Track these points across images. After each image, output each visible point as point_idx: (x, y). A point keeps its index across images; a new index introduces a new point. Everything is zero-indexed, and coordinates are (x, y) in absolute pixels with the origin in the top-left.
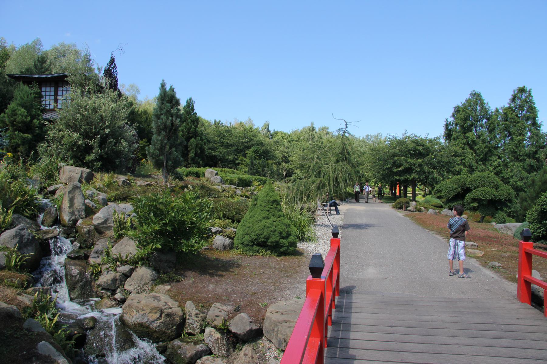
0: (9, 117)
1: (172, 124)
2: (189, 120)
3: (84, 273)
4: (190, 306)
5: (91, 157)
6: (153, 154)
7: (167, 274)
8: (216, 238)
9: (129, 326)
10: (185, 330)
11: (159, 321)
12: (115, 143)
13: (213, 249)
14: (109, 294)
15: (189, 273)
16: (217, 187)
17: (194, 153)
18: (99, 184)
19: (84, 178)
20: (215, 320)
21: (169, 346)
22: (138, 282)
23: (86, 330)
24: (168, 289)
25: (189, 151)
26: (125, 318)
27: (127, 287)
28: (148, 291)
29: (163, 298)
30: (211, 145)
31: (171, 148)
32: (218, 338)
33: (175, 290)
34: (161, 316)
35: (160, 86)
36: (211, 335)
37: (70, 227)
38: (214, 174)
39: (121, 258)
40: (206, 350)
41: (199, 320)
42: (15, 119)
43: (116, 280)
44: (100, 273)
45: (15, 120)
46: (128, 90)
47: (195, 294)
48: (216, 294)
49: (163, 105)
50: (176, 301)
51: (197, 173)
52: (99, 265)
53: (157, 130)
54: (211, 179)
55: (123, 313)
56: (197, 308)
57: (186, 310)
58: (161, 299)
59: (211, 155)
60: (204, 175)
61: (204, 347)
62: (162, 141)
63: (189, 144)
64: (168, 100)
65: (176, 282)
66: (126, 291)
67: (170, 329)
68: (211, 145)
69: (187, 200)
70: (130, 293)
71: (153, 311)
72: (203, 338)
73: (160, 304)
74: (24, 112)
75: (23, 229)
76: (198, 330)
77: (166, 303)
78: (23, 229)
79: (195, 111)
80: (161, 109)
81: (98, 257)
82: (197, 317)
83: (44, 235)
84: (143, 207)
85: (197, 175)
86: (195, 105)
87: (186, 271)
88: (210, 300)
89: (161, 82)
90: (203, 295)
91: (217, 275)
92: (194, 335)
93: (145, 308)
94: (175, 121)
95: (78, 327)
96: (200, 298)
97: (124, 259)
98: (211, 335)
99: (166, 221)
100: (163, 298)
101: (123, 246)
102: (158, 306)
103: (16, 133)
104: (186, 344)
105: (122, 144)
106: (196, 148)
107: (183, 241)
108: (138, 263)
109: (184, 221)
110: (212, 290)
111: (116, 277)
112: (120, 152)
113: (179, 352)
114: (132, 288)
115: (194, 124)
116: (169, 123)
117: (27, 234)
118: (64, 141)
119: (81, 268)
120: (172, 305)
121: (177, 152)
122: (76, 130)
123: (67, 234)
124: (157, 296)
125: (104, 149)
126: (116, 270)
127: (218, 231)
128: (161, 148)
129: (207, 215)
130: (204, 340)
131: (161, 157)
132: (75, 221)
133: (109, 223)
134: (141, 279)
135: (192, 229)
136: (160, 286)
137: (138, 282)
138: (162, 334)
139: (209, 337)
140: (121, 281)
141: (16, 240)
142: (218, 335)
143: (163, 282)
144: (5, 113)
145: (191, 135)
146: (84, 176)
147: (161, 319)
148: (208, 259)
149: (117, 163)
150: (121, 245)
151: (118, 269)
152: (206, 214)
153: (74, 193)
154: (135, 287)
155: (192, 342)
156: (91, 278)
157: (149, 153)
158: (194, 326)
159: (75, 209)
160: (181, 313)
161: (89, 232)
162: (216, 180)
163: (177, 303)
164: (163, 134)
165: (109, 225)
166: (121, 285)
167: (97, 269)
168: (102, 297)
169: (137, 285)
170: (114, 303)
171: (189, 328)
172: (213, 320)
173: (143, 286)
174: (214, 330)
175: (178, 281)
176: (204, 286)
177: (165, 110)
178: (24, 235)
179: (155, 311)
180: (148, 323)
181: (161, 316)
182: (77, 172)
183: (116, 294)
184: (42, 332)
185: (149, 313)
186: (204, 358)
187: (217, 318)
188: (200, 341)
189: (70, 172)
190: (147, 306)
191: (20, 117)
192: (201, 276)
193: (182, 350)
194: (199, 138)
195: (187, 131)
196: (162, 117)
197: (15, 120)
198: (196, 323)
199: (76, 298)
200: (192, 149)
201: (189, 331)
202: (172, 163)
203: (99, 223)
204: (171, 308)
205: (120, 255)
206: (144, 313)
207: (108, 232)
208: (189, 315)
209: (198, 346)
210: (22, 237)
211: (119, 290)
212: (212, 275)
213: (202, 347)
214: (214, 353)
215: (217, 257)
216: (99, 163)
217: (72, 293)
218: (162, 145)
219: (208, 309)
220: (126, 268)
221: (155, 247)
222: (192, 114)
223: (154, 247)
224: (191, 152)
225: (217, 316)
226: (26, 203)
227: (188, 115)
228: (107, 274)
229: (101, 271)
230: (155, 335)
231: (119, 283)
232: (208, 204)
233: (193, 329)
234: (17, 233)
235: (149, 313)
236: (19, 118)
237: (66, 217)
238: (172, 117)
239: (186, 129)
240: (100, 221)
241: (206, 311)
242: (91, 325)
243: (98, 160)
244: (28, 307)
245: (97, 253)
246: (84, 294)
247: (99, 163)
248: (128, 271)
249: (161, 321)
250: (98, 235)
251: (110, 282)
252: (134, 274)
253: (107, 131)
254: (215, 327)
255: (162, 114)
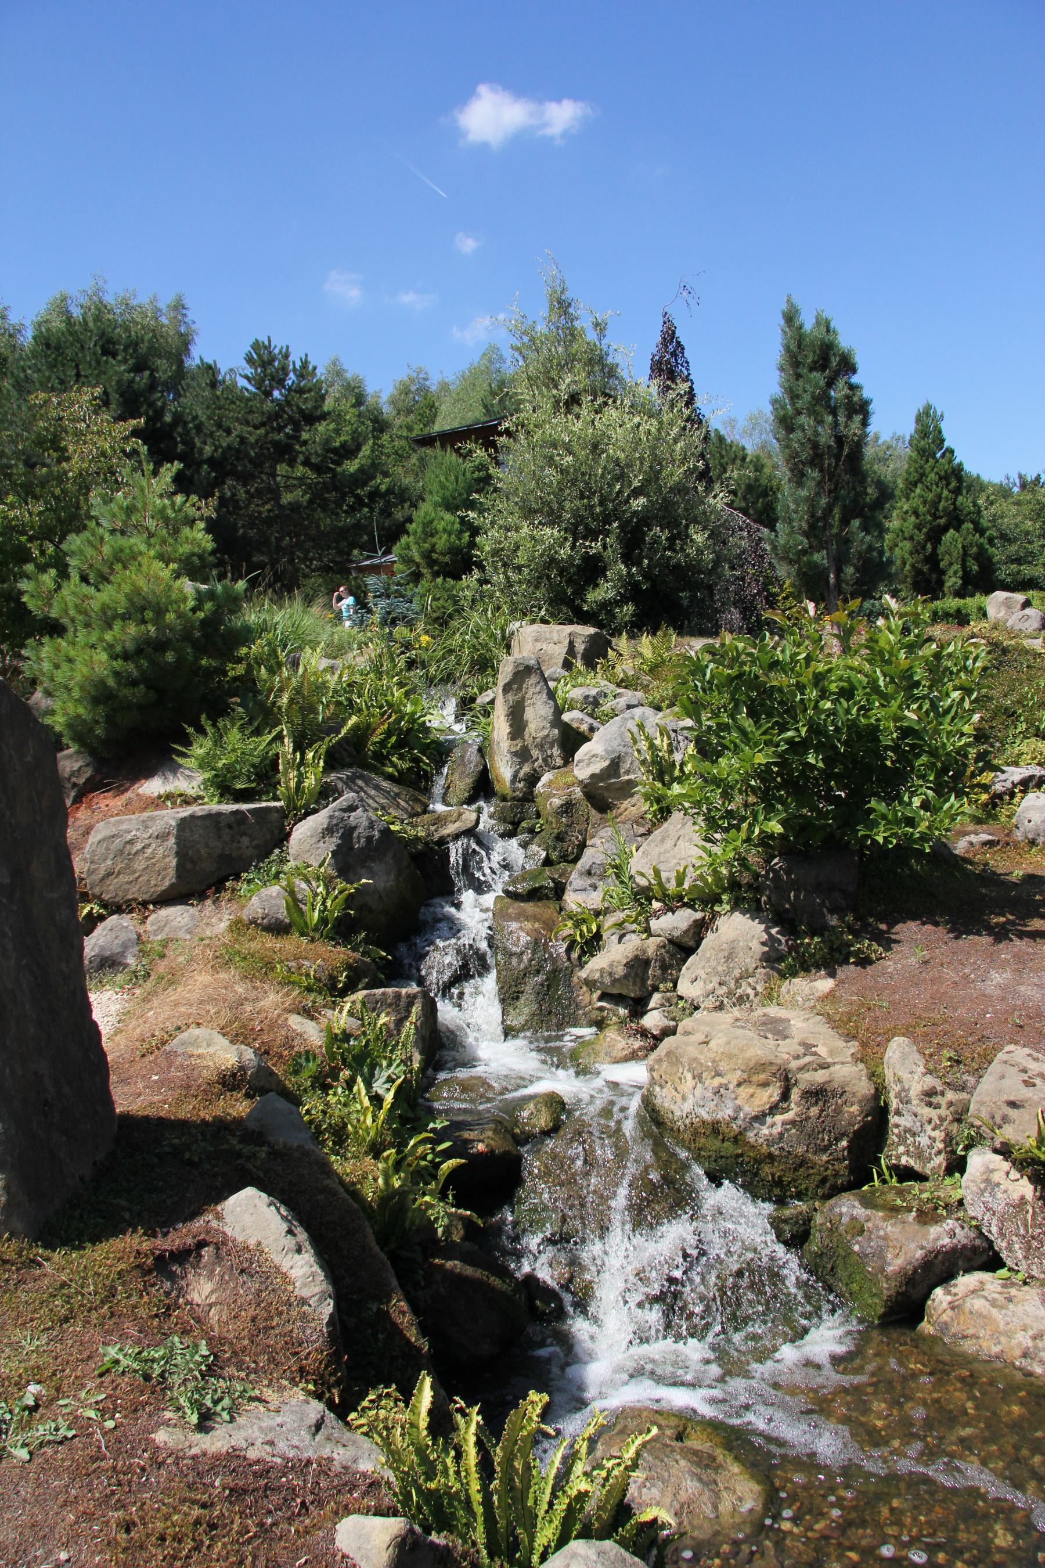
0: (417, 543)
1: (840, 440)
2: (932, 476)
3: (546, 944)
4: (904, 1057)
5: (603, 592)
6: (787, 550)
7: (821, 935)
8: (1024, 803)
9: (675, 1132)
10: (889, 1157)
11: (779, 1118)
12: (671, 540)
13: (1016, 844)
14: (623, 1011)
15: (908, 930)
16: (1030, 641)
17: (960, 574)
18: (625, 667)
19: (579, 656)
20: (1005, 1119)
21: (818, 1219)
22: (720, 969)
23: (524, 1139)
24: (827, 990)
25: (943, 572)
26: (658, 1101)
27: (684, 987)
28: (756, 1000)
29: (800, 1025)
30: (1013, 549)
31: (845, 522)
32: (1022, 1198)
33: (849, 996)
34: (785, 1096)
35: (782, 322)
36: (990, 1185)
37: (519, 800)
38: (1019, 606)
39: (660, 884)
40: (974, 1249)
41: (942, 1119)
42: (434, 545)
43: (647, 963)
44: (593, 944)
45: (433, 549)
46: (745, 432)
47: (926, 1009)
48: (1014, 1008)
49: (801, 383)
50: (850, 1037)
51: (959, 611)
52: (597, 913)
53: (792, 470)
54: (1009, 624)
55: (653, 1082)
56: (931, 1066)
57: (889, 1074)
58: (794, 1031)
59: (1020, 578)
60: (985, 615)
61: (964, 1236)
62: (811, 501)
63: (941, 549)
64: (814, 362)
65: (855, 964)
66: (681, 1004)
67: (825, 1149)
68: (1013, 549)
69: (881, 653)
70: (697, 1008)
71: (755, 1078)
72: (957, 1195)
73: (784, 1051)
74: (453, 524)
75: (352, 808)
76: (940, 1161)
77: (808, 1047)
78: (352, 808)
79: (946, 444)
80: (794, 396)
81: (595, 887)
82: (929, 1104)
83: (432, 828)
84: (711, 689)
85: (961, 618)
86: (943, 426)
87: (897, 922)
88: (986, 1033)
89: (784, 307)
90: (961, 1012)
91: (1021, 935)
92: (922, 1178)
93: (723, 1067)
94: (846, 426)
95: (495, 1131)
96: (946, 1027)
97: (672, 887)
98: (990, 1185)
99: (797, 730)
100: (800, 1025)
101: (669, 843)
102: (771, 1058)
103: (439, 580)
104: (884, 1219)
105: (692, 540)
106: (964, 561)
107: (873, 803)
108: (720, 902)
109: (874, 731)
110: (998, 992)
111: (644, 952)
112: (689, 566)
113: (856, 1248)
114: (699, 993)
115: (948, 484)
116: (825, 436)
117: (365, 823)
118: (522, 558)
119: (537, 925)
120: (831, 1053)
121: (868, 532)
122: (554, 519)
123: (512, 823)
124: (780, 1020)
125: (639, 564)
126: (647, 930)
127: (1031, 777)
128: (812, 526)
129: (962, 700)
130: (961, 1203)
131: (816, 557)
132: (533, 779)
133: (628, 772)
134: (729, 958)
135: (905, 758)
136: (796, 981)
137: (720, 969)
138: (796, 1170)
139: (983, 1191)
140: (664, 967)
141: (332, 843)
142: (1025, 1188)
143: (804, 966)
144: (408, 533)
145: (942, 521)
146: (580, 647)
147: (787, 1110)
148: (990, 878)
149: (685, 603)
150: (663, 840)
151: (654, 924)
152: (956, 695)
153: (520, 689)
154: (710, 987)
155: (909, 1210)
156: (569, 959)
157: (774, 548)
158: (924, 1141)
159: (529, 741)
160: (864, 1088)
161: (568, 807)
162: (1026, 625)
163: (854, 1047)
164: (814, 479)
165: (626, 778)
166: (664, 980)
167: (584, 928)
168: (600, 1024)
169: (716, 980)
170: (637, 1043)
171: (901, 1149)
172: (998, 1120)
173: (737, 981)
174: (1006, 1165)
175: (864, 962)
176: (966, 977)
177: (807, 397)
178: (355, 828)
179: (762, 1077)
180: (739, 1122)
181: (785, 1096)
182: (556, 638)
183: (645, 1013)
184: (300, 1147)
185: (739, 1085)
186: (965, 1282)
187: (1013, 1113)
188: (946, 1206)
189: (537, 640)
190: (730, 1056)
191: (445, 536)
192: (957, 938)
193: (870, 1239)
194: (971, 526)
195: (929, 511)
196: (803, 419)
197: (433, 549)
198: (928, 1128)
199: (522, 1029)
200: (951, 564)
201: (904, 1160)
202: (857, 570)
203: (593, 776)
204: (825, 1066)
205: (657, 873)
206: (721, 1085)
207: (626, 803)
208: (898, 1096)
209: (934, 1230)
210: (348, 833)
211: (656, 999)
212: (1000, 935)
213: (953, 1234)
214: (1009, 1262)
215: (1031, 870)
216: (629, 609)
217: (511, 1009)
218: (813, 515)
219: (978, 1073)
220: (680, 921)
221: (762, 832)
222: (938, 455)
223: (757, 831)
224: (951, 572)
225: (1013, 1104)
226: (394, 739)
227: (927, 461)
228: (620, 942)
229: (598, 936)
230: (767, 1170)
231: (658, 972)
232: (967, 658)
233: (919, 1155)
234: (334, 822)
235: (739, 1085)
236: (442, 542)
237: (504, 770)
238: (835, 415)
239: (925, 502)
240: (597, 767)
241: (971, 1080)
242: (543, 1121)
243: (623, 600)
244: (309, 1055)
245: (589, 873)
246: (550, 1013)
247: (629, 609)
248: (686, 932)
249: (789, 1116)
250: (599, 816)
251: (620, 971)
252: (709, 940)
253: (639, 503)
254: (1005, 1151)
255: (799, 413)
